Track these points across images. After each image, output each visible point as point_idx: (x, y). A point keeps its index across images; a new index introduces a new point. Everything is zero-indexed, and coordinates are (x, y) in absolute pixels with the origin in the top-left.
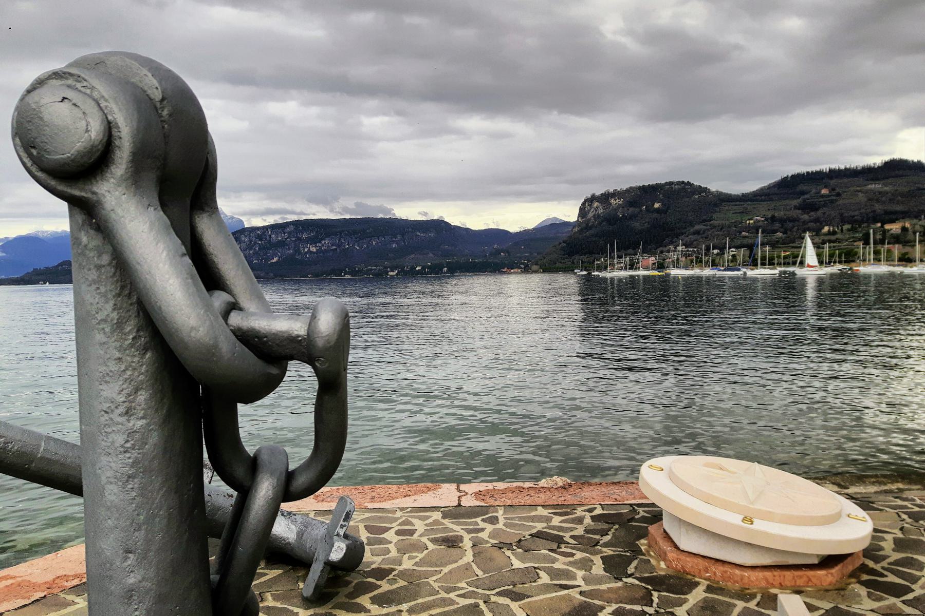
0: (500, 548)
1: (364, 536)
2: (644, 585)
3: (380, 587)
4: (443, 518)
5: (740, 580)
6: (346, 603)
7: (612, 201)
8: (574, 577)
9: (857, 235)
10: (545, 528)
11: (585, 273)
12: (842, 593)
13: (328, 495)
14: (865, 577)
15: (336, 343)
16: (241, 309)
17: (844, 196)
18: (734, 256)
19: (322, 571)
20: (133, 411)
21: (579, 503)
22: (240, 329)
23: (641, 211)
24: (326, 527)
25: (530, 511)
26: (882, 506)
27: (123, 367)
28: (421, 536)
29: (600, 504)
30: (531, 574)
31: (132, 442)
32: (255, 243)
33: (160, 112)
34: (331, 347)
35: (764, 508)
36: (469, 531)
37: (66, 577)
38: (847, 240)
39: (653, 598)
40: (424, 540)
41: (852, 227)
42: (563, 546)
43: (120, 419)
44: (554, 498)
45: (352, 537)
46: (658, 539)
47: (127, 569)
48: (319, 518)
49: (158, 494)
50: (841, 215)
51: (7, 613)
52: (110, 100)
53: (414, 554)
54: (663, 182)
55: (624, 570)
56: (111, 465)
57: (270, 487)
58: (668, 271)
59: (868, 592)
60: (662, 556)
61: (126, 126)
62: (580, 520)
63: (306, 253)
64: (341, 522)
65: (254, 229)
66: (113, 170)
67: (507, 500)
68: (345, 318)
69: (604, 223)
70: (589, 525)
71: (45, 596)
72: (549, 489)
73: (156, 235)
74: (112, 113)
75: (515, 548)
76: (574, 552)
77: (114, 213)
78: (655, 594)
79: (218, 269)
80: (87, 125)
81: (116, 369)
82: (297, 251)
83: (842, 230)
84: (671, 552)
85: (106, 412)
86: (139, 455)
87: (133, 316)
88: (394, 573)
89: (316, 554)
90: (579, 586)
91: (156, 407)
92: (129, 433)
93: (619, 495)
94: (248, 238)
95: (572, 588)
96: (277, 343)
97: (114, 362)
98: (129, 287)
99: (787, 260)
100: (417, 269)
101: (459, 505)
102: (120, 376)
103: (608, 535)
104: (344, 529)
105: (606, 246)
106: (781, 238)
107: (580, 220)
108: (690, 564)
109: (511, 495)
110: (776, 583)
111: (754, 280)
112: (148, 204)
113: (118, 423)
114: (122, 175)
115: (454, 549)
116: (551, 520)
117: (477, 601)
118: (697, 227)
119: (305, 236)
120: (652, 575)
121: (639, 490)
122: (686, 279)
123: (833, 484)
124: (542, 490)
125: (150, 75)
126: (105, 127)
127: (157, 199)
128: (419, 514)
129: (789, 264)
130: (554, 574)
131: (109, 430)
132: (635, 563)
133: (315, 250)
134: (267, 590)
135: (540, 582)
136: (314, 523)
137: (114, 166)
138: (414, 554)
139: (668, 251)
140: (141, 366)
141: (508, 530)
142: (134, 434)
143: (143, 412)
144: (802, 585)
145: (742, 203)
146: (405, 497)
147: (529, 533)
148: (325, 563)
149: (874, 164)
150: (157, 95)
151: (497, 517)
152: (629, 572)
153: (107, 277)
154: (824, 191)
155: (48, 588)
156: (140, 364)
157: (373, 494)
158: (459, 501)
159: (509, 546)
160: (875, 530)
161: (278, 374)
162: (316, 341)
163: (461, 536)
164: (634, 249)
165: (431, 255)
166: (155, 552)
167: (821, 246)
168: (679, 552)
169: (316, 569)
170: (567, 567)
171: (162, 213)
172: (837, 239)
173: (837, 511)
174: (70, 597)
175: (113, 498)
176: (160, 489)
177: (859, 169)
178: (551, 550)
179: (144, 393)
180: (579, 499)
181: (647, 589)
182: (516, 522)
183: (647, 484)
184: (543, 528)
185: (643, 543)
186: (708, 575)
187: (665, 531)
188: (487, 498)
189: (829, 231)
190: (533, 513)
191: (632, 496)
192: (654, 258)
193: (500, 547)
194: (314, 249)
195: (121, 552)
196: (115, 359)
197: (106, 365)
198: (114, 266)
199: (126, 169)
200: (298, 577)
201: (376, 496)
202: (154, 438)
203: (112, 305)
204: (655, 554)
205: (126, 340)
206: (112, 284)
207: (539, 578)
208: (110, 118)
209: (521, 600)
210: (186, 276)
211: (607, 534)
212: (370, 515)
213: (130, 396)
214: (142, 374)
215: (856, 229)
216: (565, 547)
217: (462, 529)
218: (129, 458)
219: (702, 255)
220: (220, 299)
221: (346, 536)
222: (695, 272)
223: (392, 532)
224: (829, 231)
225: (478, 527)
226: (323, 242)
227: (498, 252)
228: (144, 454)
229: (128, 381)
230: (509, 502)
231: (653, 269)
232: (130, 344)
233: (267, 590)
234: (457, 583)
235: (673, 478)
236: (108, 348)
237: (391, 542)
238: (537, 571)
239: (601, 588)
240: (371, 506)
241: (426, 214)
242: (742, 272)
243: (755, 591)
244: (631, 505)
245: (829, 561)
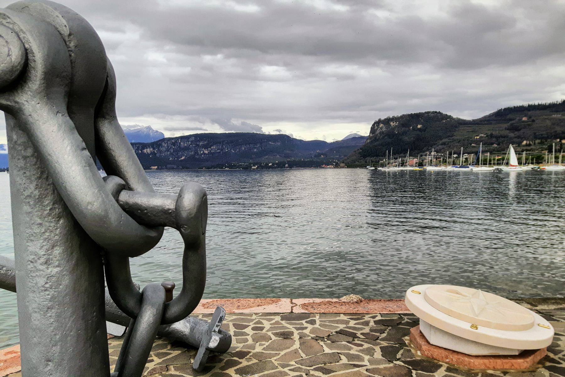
0: (317, 340)
1: (232, 331)
2: (407, 366)
3: (241, 363)
4: (282, 320)
5: (468, 364)
6: (219, 373)
7: (392, 123)
8: (363, 360)
9: (544, 146)
10: (345, 328)
11: (373, 168)
12: (533, 374)
13: (211, 304)
14: (548, 364)
15: (195, 215)
16: (130, 189)
17: (536, 122)
18: (466, 159)
19: (204, 354)
20: (51, 261)
21: (366, 312)
22: (127, 203)
23: (410, 129)
24: (208, 325)
25: (336, 317)
26: (559, 318)
27: (43, 230)
28: (268, 331)
29: (380, 313)
30: (336, 357)
31: (50, 284)
32: (171, 148)
33: (68, 44)
34: (192, 218)
35: (484, 319)
36: (297, 329)
38: (537, 150)
39: (412, 374)
40: (270, 333)
41: (541, 141)
42: (356, 339)
43: (41, 267)
44: (351, 309)
45: (224, 332)
46: (416, 337)
47: (48, 373)
48: (205, 319)
49: (69, 320)
50: (535, 134)
51: (10, 375)
52: (28, 33)
53: (263, 343)
54: (423, 112)
55: (394, 356)
56: (35, 299)
57: (151, 315)
58: (425, 168)
59: (550, 374)
60: (419, 348)
61: (39, 52)
62: (367, 323)
63: (202, 154)
64: (217, 323)
65: (170, 139)
66: (30, 85)
67: (321, 310)
68: (204, 197)
69: (386, 137)
70: (373, 326)
72: (348, 303)
73: (62, 134)
74: (28, 42)
75: (326, 340)
76: (363, 343)
77: (32, 117)
78: (414, 372)
79: (115, 160)
80: (9, 51)
81: (38, 231)
82: (196, 153)
83: (535, 144)
84: (425, 345)
85: (32, 262)
86: (55, 293)
87: (50, 193)
88: (250, 354)
89: (202, 342)
90: (366, 366)
91: (67, 259)
92: (48, 277)
93: (392, 308)
94: (166, 144)
95: (361, 367)
96: (154, 214)
97: (36, 226)
98: (47, 172)
99: (499, 162)
100: (269, 165)
101: (292, 312)
102: (41, 236)
103: (385, 333)
104: (219, 327)
105: (386, 151)
106: (496, 147)
107: (371, 135)
108: (436, 353)
109: (324, 306)
110: (491, 367)
111: (477, 174)
112: (57, 111)
113: (40, 270)
114: (37, 89)
115: (288, 340)
116: (349, 323)
117: (301, 373)
118: (444, 140)
119: (201, 143)
120: (412, 359)
121: (405, 305)
122: (438, 173)
123: (528, 303)
124: (343, 304)
125: (60, 16)
126: (22, 53)
127: (65, 108)
128: (267, 317)
129: (500, 164)
130: (350, 357)
131: (34, 275)
132: (401, 352)
133: (207, 153)
134: (171, 363)
135: (341, 362)
136: (200, 323)
137: (31, 82)
138: (263, 343)
139: (426, 155)
140: (57, 229)
141: (322, 328)
142: (52, 278)
143: (57, 262)
144: (507, 368)
145: (472, 126)
146: (258, 306)
147: (335, 331)
148: (206, 349)
149: (557, 102)
150: (66, 31)
151: (315, 320)
152: (398, 357)
153: (31, 165)
154: (524, 119)
156: (56, 228)
157: (239, 304)
158: (292, 309)
159: (322, 339)
160: (556, 334)
161: (155, 236)
162: (181, 214)
163: (293, 332)
164: (404, 154)
165: (278, 156)
166: (68, 361)
167: (521, 153)
168: (429, 346)
169: (201, 351)
170: (358, 353)
171: (68, 118)
172: (531, 149)
173: (532, 322)
175: (37, 323)
176: (71, 316)
177: (547, 104)
178: (348, 342)
179: (58, 249)
180: (367, 310)
181: (409, 368)
182: (327, 323)
183: (410, 302)
184: (344, 328)
185: (406, 339)
186: (448, 360)
187: (421, 332)
188: (309, 308)
189: (526, 144)
190: (338, 318)
191: (400, 309)
192: (416, 160)
193: (317, 339)
194: (206, 152)
195: (44, 360)
196: (38, 224)
197: (31, 229)
198: (35, 157)
199: (40, 85)
200: (190, 356)
201: (241, 305)
202: (66, 281)
203: (34, 185)
204: (414, 346)
205: (45, 210)
206: (35, 170)
207: (341, 360)
208: (27, 46)
209: (329, 373)
210: (84, 164)
211: (384, 333)
212: (236, 317)
213: (49, 250)
214: (57, 235)
215: (544, 142)
216: (358, 340)
217: (293, 327)
218: (48, 295)
219: (446, 158)
220: (115, 181)
221: (220, 332)
222: (442, 168)
223: (250, 328)
224: (526, 144)
225: (303, 326)
226: (212, 147)
227: (319, 155)
228: (59, 292)
229: (46, 240)
230: (323, 311)
231: (416, 166)
232: (48, 213)
233: (171, 363)
234: (290, 361)
235: (426, 298)
236: (32, 216)
237: (249, 335)
238: (340, 355)
239: (379, 367)
240: (237, 311)
241: (279, 131)
242: (470, 169)
243: (477, 371)
244: (399, 314)
245: (525, 354)
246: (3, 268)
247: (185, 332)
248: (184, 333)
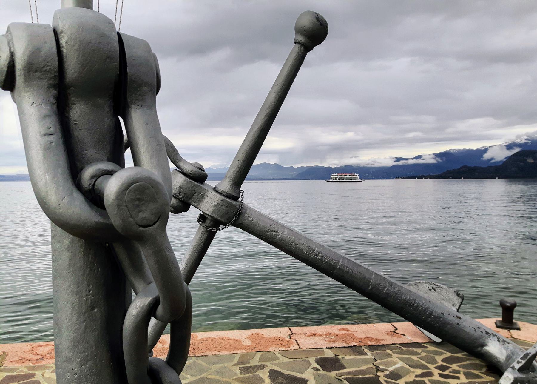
37: (370, 339)
71: (356, 345)
155: (360, 342)
174: (366, 350)
246: (319, 254)
247: (500, 358)
248: (499, 360)
